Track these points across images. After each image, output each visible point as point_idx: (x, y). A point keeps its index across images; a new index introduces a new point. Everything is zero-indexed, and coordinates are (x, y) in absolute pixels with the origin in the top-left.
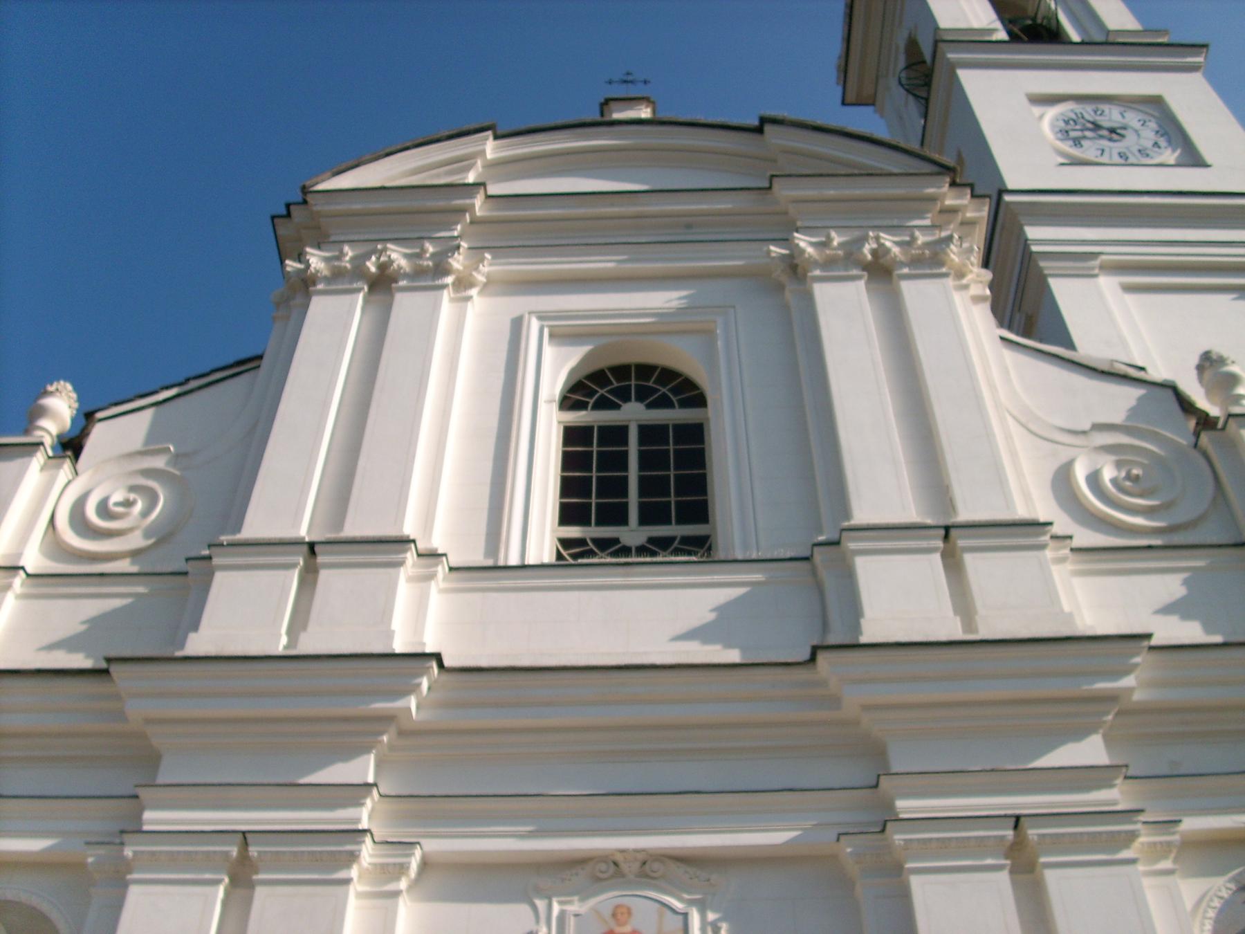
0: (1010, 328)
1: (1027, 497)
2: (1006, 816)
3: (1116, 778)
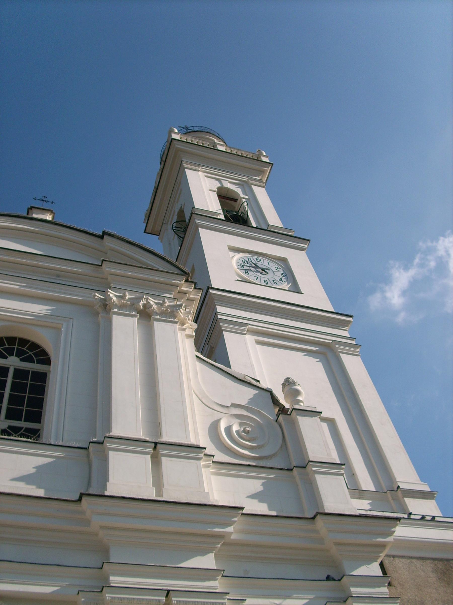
0: (202, 353)
1: (196, 433)
2: (163, 590)
3: (218, 576)
